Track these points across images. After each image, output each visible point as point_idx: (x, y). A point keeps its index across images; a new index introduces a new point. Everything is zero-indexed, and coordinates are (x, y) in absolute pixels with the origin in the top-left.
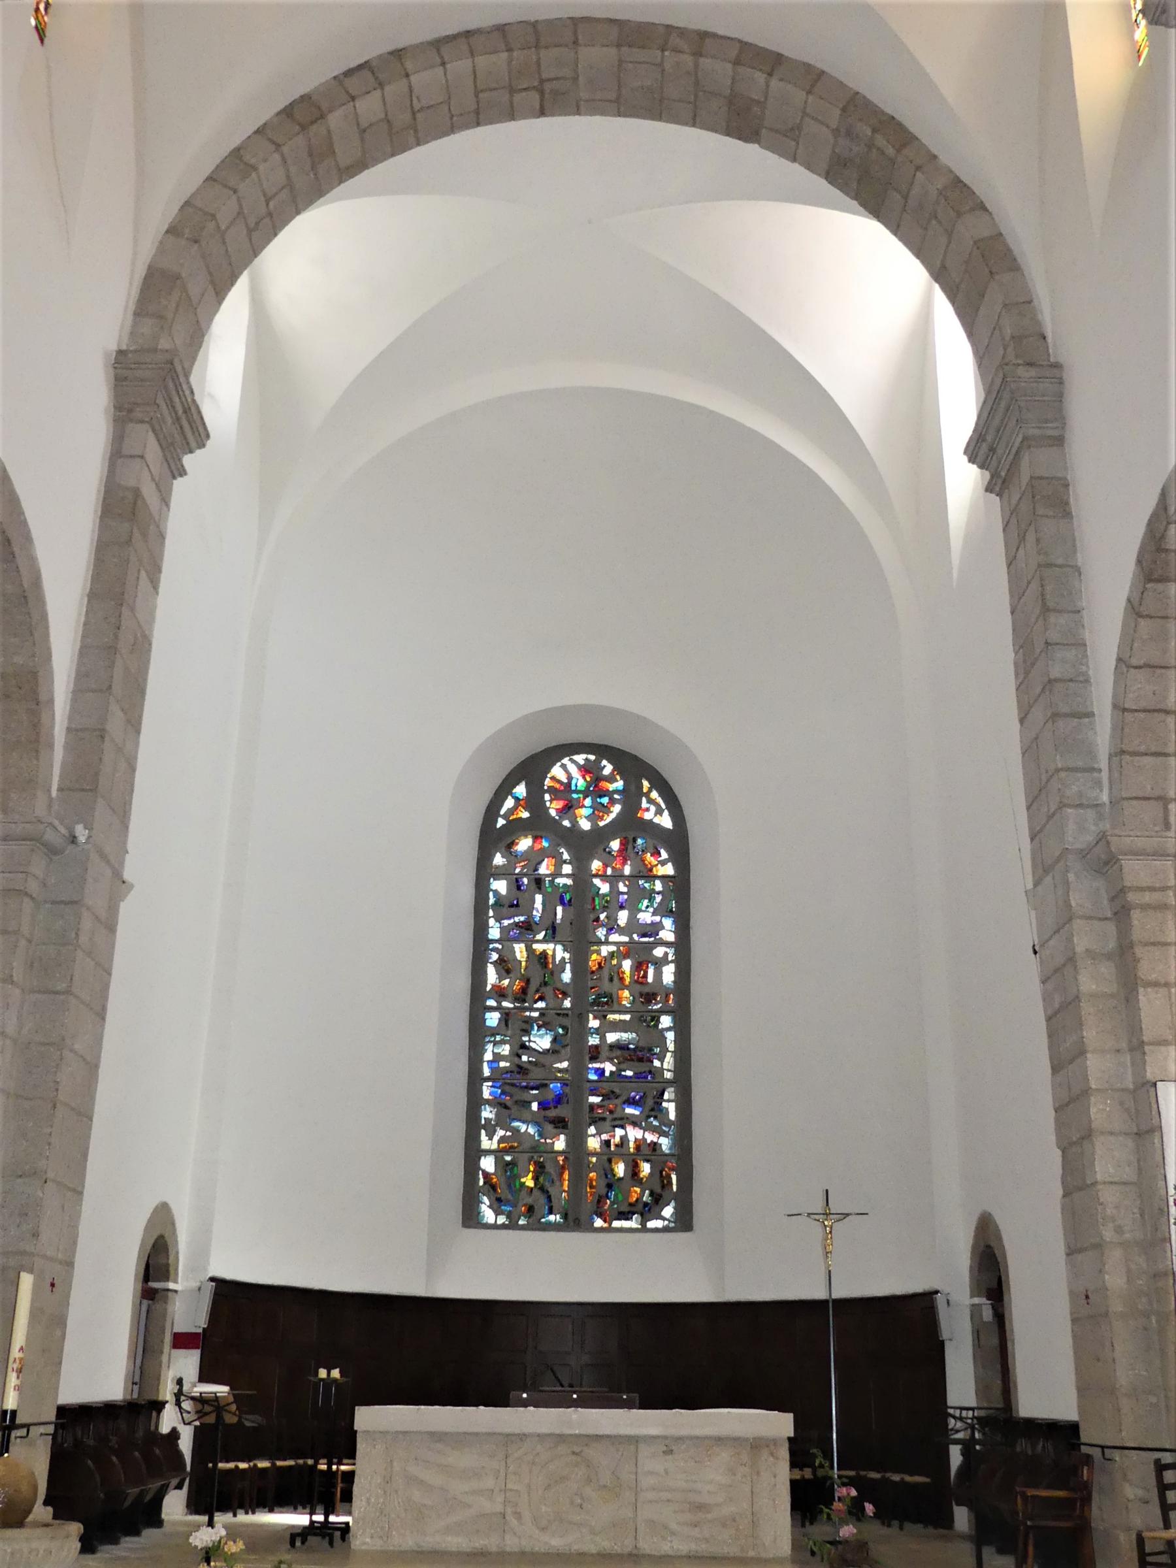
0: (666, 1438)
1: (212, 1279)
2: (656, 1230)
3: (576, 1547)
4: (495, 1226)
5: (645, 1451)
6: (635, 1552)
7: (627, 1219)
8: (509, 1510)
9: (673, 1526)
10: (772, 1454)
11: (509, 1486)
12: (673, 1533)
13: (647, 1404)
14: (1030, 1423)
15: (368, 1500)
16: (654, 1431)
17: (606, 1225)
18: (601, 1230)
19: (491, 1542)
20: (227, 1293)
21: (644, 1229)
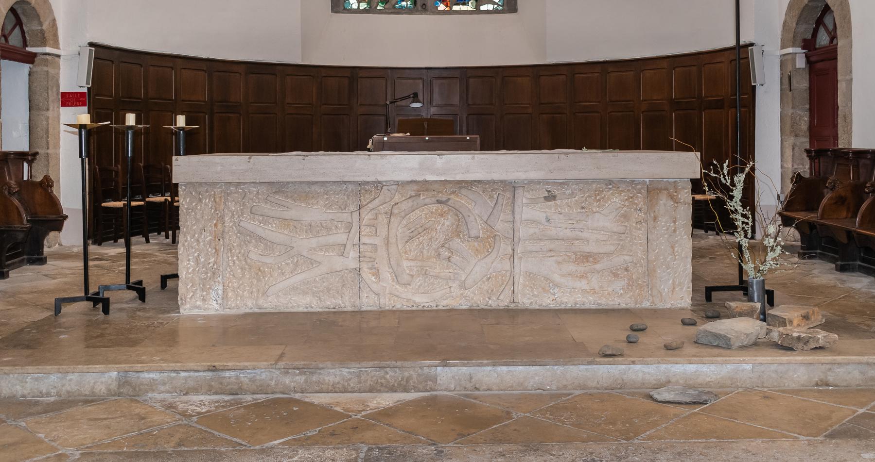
0: (546, 182)
1: (91, 44)
2: (488, 12)
3: (445, 303)
4: (358, 11)
5: (523, 198)
6: (512, 306)
7: (464, 4)
8: (365, 267)
9: (556, 278)
10: (672, 197)
11: (364, 240)
12: (557, 285)
13: (487, 145)
14: (860, 154)
15: (197, 260)
16: (533, 175)
17: (448, 9)
18: (444, 12)
19: (346, 302)
20: (106, 58)
21: (478, 11)
